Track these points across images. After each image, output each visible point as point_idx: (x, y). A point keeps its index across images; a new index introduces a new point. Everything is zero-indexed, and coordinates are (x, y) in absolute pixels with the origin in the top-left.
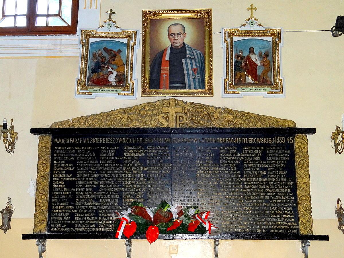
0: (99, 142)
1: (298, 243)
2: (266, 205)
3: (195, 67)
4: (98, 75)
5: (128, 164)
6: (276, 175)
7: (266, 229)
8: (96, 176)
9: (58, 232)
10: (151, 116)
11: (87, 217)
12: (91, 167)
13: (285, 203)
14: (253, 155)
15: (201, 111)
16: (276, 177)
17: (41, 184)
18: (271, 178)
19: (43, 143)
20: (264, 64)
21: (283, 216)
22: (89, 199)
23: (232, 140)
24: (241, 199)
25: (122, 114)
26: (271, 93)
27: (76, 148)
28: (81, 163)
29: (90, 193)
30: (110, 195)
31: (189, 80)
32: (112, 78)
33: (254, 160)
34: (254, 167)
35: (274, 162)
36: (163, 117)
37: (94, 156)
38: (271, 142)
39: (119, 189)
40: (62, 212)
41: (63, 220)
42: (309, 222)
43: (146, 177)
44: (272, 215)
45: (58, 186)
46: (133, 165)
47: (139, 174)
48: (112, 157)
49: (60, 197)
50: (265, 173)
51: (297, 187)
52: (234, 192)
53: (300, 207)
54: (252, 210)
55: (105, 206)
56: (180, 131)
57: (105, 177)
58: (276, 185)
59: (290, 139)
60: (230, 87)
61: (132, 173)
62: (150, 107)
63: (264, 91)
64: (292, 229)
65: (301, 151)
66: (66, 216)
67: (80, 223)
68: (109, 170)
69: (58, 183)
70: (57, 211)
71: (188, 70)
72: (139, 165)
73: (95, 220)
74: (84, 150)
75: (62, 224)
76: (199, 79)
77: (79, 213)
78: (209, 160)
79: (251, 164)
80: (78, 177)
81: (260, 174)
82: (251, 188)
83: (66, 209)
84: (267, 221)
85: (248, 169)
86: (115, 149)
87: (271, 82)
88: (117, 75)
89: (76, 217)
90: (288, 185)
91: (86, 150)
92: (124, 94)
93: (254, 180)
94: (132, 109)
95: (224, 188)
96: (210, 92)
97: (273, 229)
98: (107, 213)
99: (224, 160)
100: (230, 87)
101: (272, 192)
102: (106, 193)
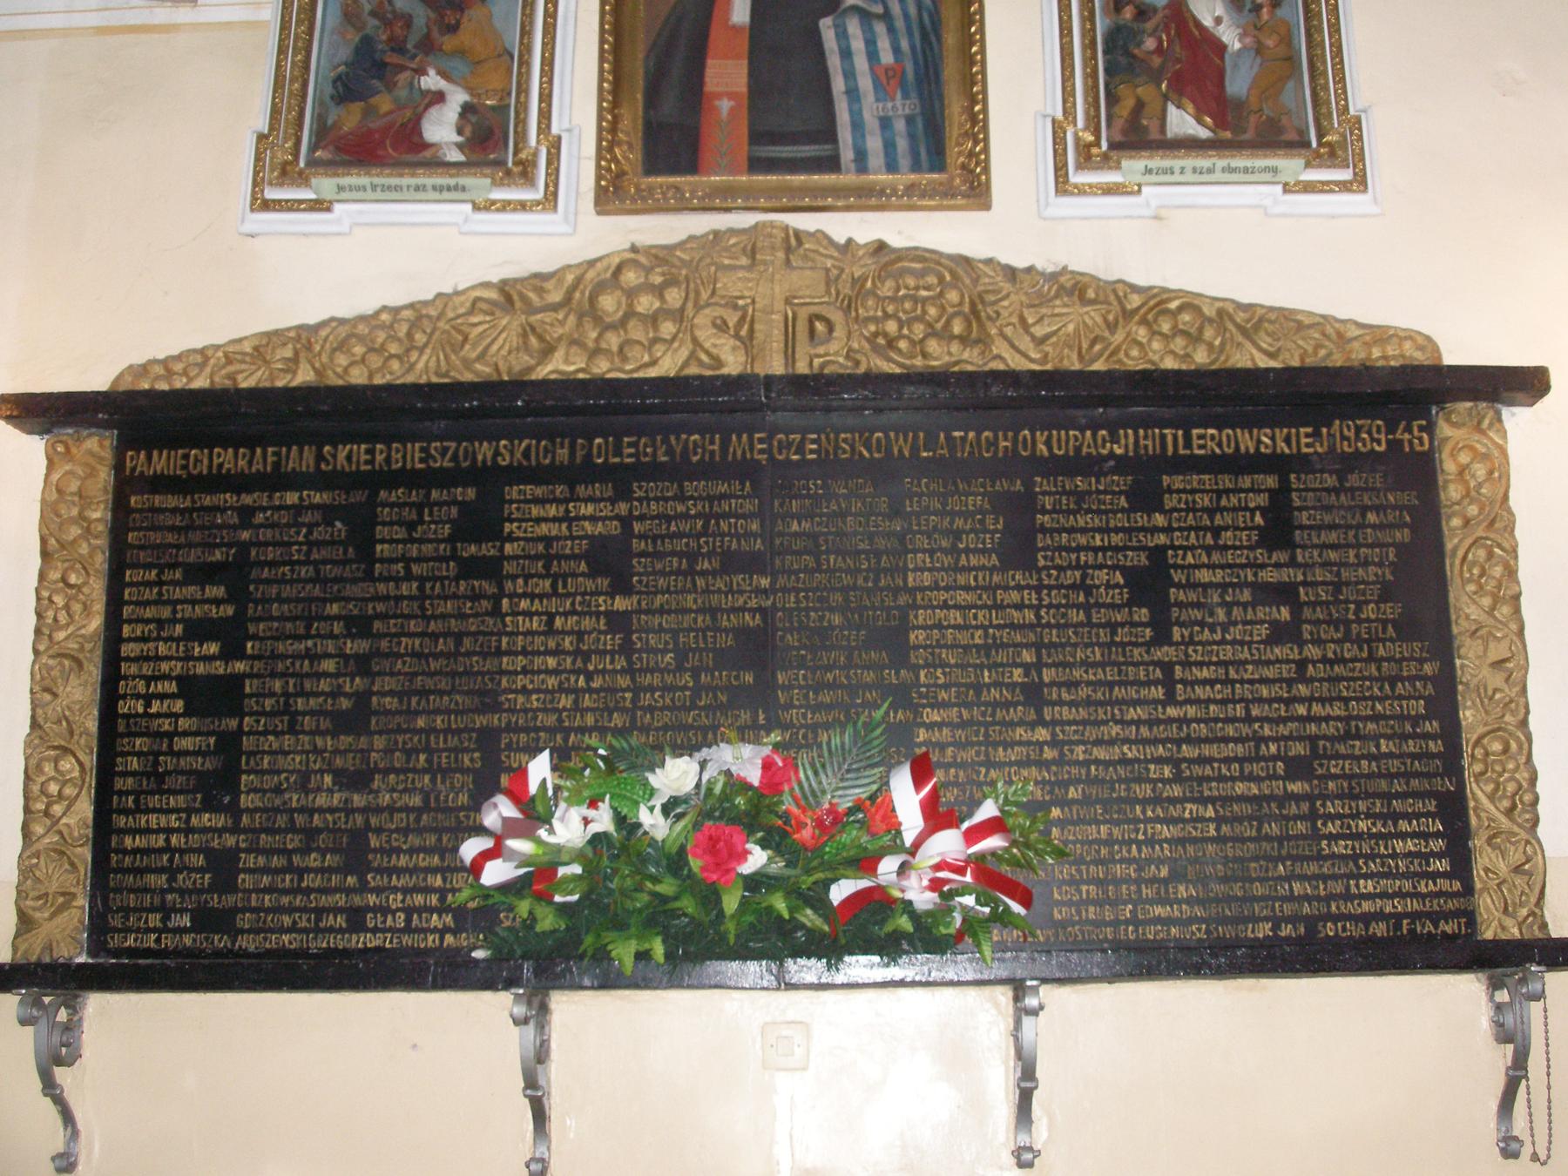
0: (367, 463)
1: (1464, 993)
2: (1296, 787)
3: (887, 58)
4: (369, 112)
5: (526, 583)
6: (1347, 623)
7: (1294, 920)
8: (350, 647)
9: (148, 953)
10: (653, 320)
11: (301, 872)
12: (324, 600)
13: (1397, 775)
14: (1218, 521)
15: (927, 288)
16: (1347, 638)
17: (55, 695)
18: (1318, 642)
19: (67, 473)
20: (1259, 42)
21: (1386, 848)
22: (316, 772)
23: (1104, 441)
24: (1159, 761)
25: (492, 314)
26: (1308, 188)
27: (247, 499)
28: (268, 582)
29: (319, 741)
30: (428, 749)
31: (857, 126)
32: (442, 129)
33: (1226, 548)
34: (1224, 586)
35: (1333, 555)
36: (721, 326)
37: (340, 543)
38: (1311, 450)
39: (480, 721)
40: (168, 849)
41: (171, 890)
42: (1525, 873)
43: (627, 649)
44: (1329, 845)
45: (148, 705)
46: (554, 586)
47: (590, 633)
48: (440, 541)
49: (156, 763)
50: (1285, 614)
51: (1460, 687)
52: (1117, 722)
53: (1479, 793)
54: (1219, 820)
55: (400, 810)
56: (813, 390)
57: (402, 656)
58: (1344, 679)
59: (1411, 432)
60: (1086, 159)
61: (550, 630)
62: (648, 270)
63: (1267, 177)
64: (1435, 917)
65: (1473, 493)
66: (191, 870)
67: (267, 903)
68: (424, 617)
69: (148, 687)
70: (140, 842)
71: (850, 74)
72: (589, 585)
73: (349, 891)
74: (287, 508)
75: (166, 911)
76: (910, 120)
77: (259, 851)
78: (976, 551)
79: (1208, 567)
80: (253, 657)
81: (1256, 623)
82: (1209, 701)
83: (188, 831)
84: (1303, 878)
85: (1193, 596)
86: (455, 502)
87: (1303, 133)
88: (467, 110)
89: (242, 876)
90: (1412, 679)
91: (298, 509)
92: (505, 206)
93: (1227, 653)
94: (549, 285)
95: (1061, 703)
96: (972, 188)
97: (1335, 918)
98: (412, 851)
99: (1060, 549)
100: (1089, 157)
101: (1327, 719)
102: (405, 743)
